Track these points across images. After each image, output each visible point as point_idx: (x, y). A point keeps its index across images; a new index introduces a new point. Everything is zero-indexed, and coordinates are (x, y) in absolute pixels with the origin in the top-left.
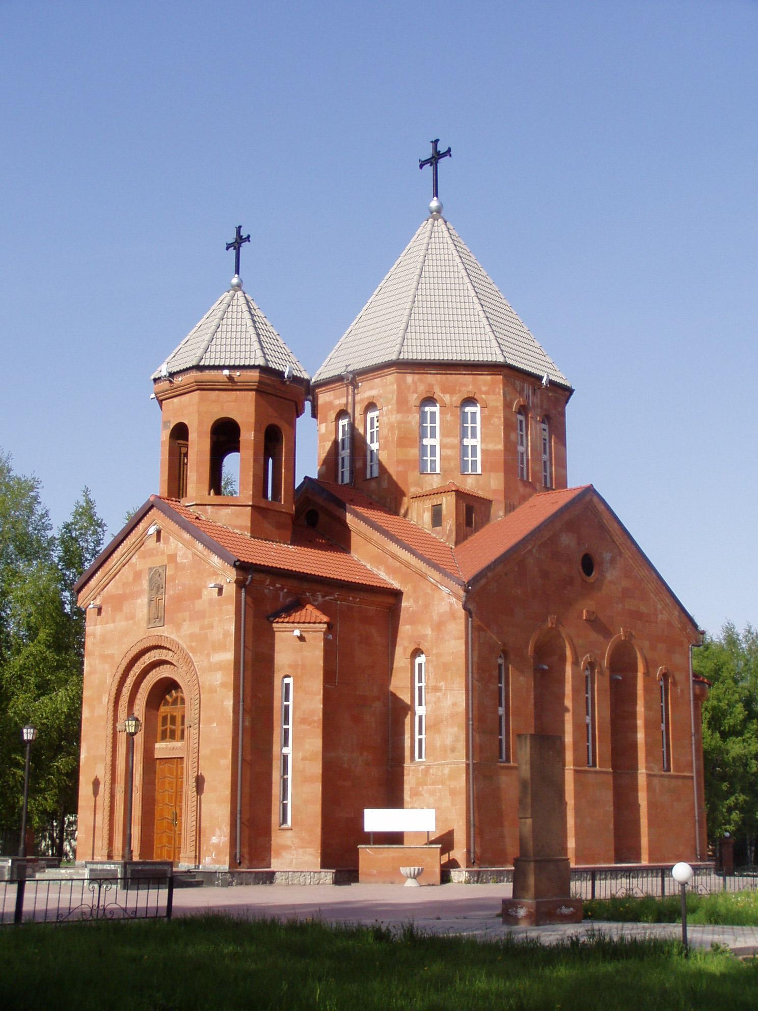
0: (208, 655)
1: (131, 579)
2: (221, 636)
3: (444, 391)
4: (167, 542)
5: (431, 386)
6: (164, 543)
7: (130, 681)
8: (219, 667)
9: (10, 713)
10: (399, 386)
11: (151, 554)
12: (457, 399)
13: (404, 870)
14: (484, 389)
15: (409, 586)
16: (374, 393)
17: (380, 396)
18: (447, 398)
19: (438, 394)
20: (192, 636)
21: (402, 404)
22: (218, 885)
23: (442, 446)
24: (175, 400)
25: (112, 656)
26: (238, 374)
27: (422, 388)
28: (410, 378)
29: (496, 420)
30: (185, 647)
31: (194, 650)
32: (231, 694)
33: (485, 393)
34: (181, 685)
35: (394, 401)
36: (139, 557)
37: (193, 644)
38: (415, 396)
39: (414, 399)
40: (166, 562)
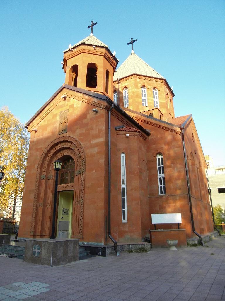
0: (90, 141)
1: (51, 118)
2: (97, 132)
3: (148, 84)
4: (69, 101)
5: (144, 83)
6: (68, 101)
7: (48, 158)
8: (97, 145)
9: (62, 262)
10: (135, 82)
11: (61, 107)
12: (152, 87)
13: (171, 242)
14: (159, 86)
15: (153, 132)
16: (126, 84)
17: (129, 85)
18: (149, 87)
19: (146, 85)
20: (81, 135)
21: (136, 86)
22: (99, 255)
23: (148, 99)
24: (72, 59)
25: (41, 148)
26: (98, 49)
27: (141, 83)
28: (138, 80)
29: (163, 94)
30: (77, 139)
31: (82, 140)
32: (104, 156)
33: (159, 87)
34: (74, 159)
35: (134, 85)
36: (56, 109)
37: (82, 138)
38: (140, 85)
39: (140, 85)
40: (68, 108)
